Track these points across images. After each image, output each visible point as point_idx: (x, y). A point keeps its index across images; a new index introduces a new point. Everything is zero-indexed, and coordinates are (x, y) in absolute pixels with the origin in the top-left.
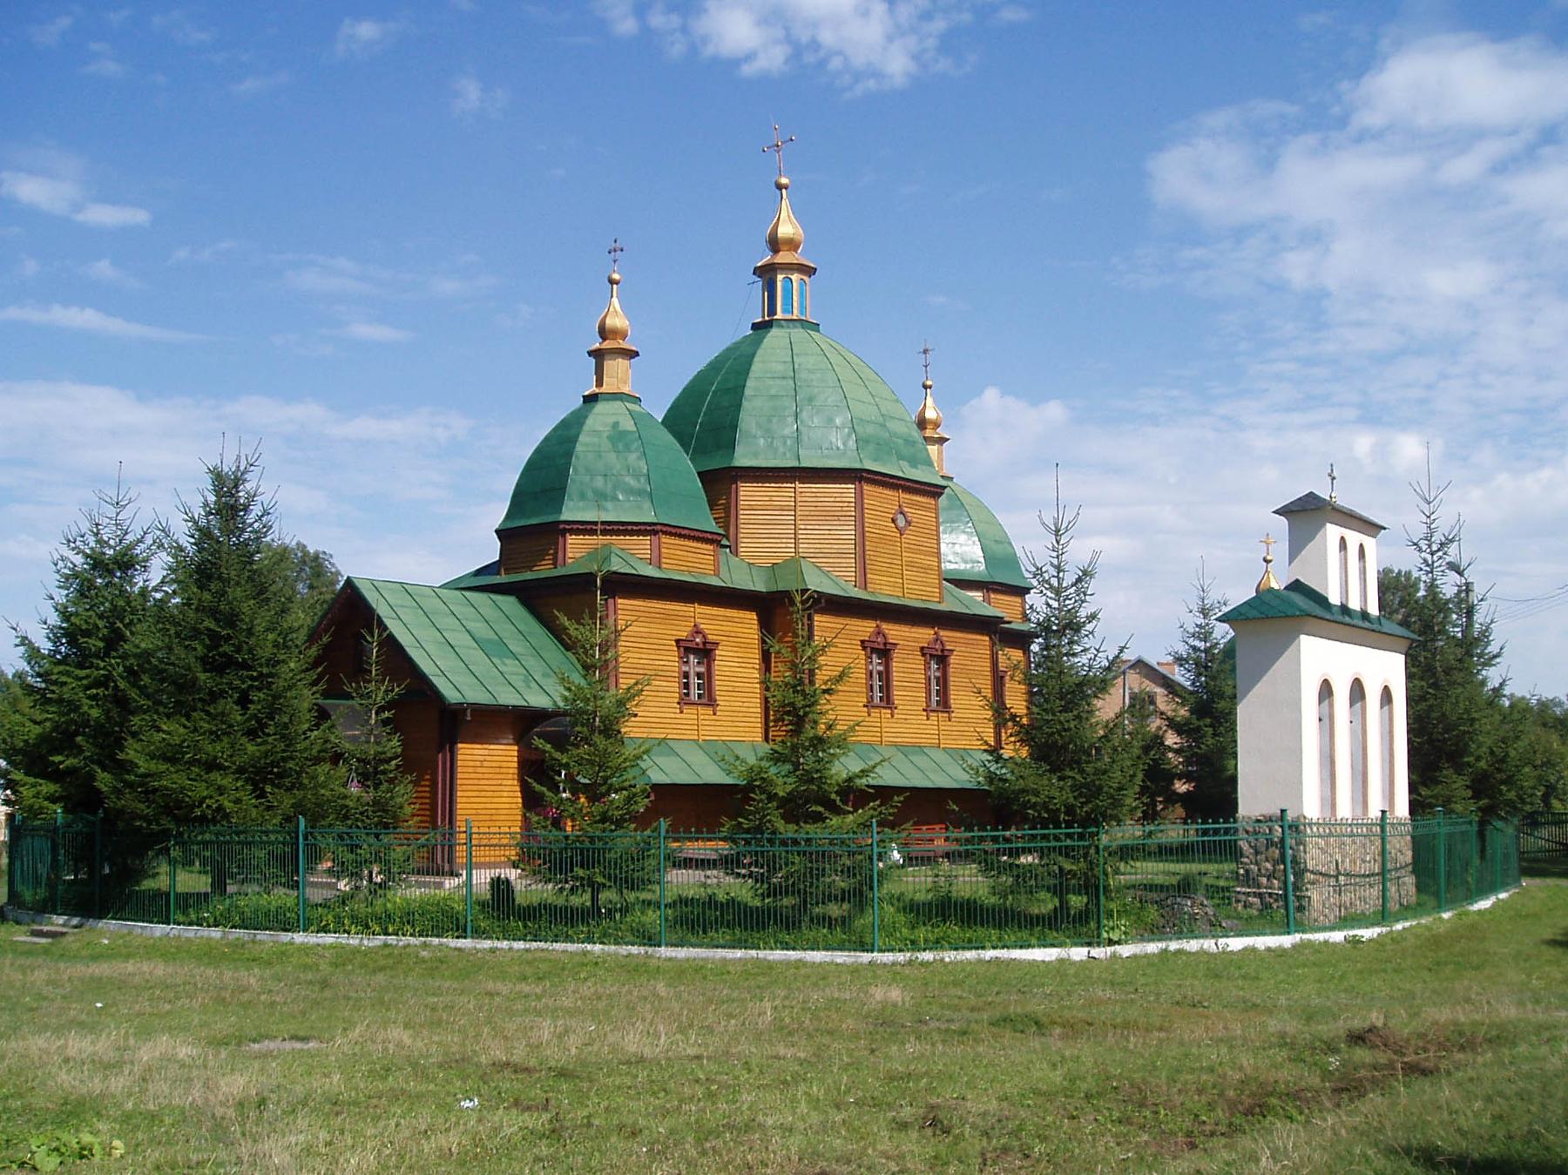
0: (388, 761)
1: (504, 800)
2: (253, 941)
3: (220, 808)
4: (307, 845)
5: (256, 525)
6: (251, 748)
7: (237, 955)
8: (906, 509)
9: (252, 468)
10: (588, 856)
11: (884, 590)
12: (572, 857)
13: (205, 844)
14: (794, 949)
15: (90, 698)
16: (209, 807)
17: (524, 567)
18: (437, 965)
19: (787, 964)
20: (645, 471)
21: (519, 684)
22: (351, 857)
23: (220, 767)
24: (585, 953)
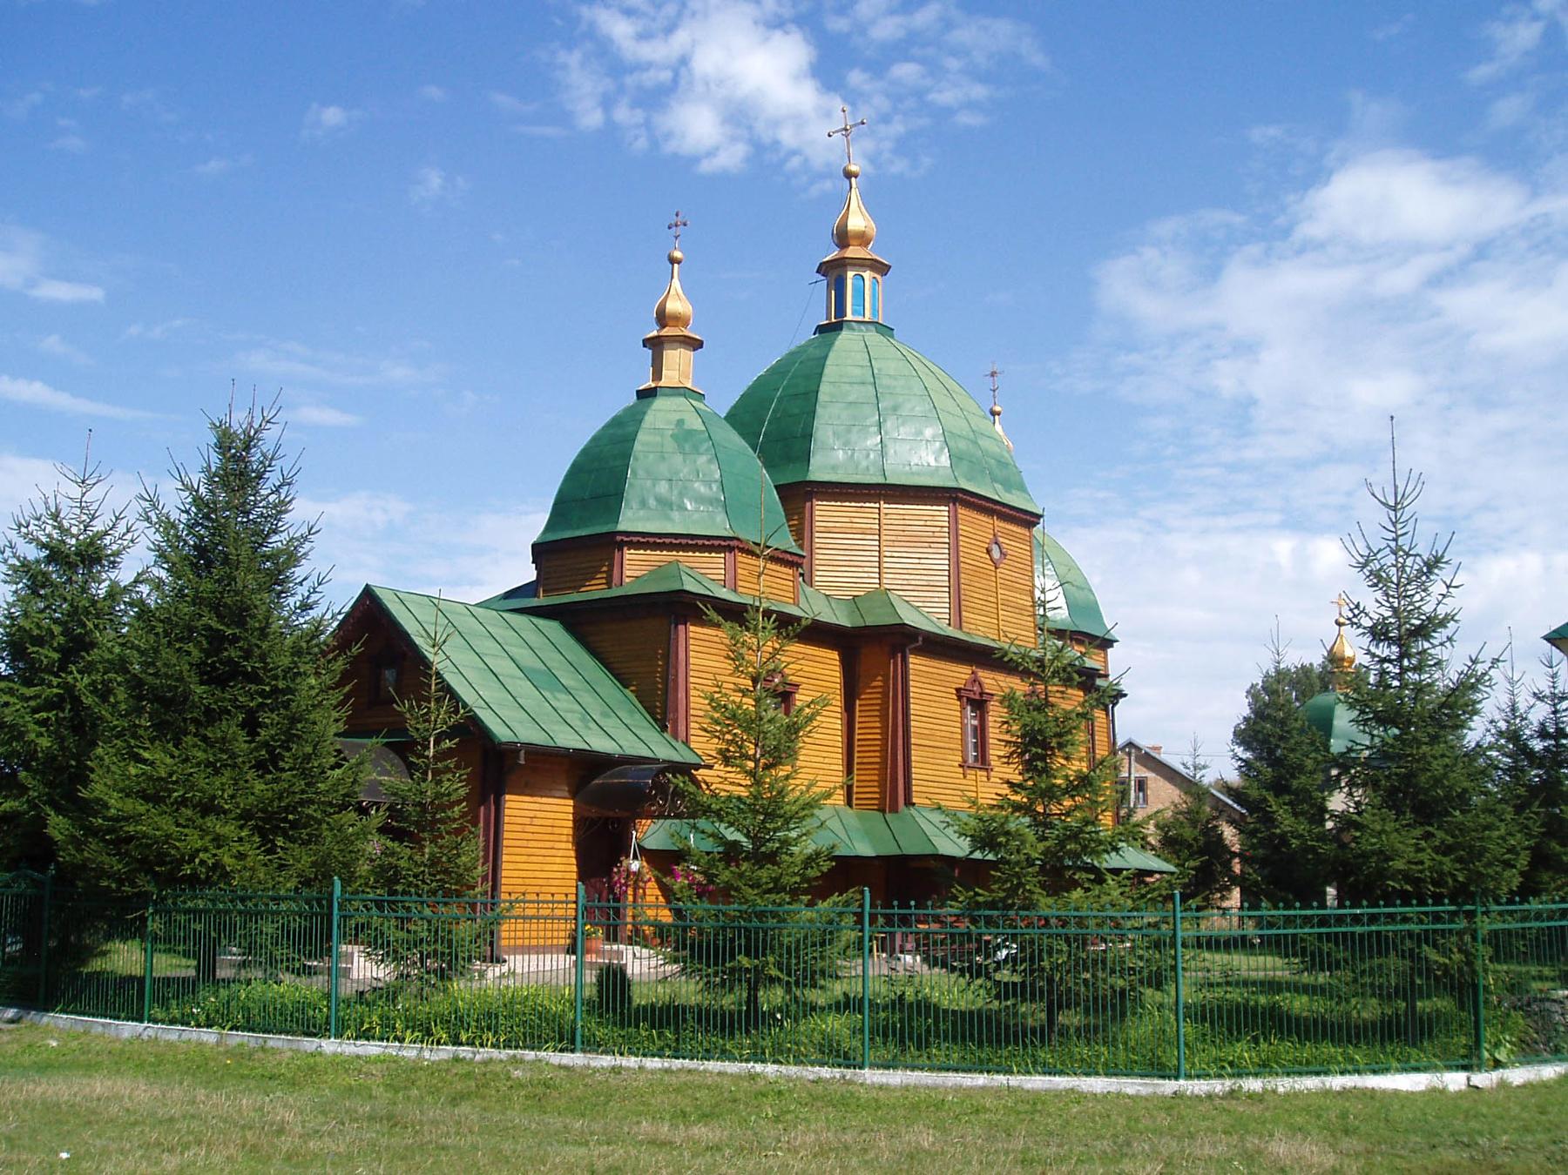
0: (452, 805)
1: (555, 867)
2: (263, 1049)
3: (217, 865)
4: (345, 917)
5: (272, 498)
6: (259, 786)
7: (241, 1070)
8: (1001, 540)
9: (269, 426)
10: (757, 940)
11: (979, 630)
12: (732, 940)
13: (196, 913)
14: (1061, 1073)
15: (39, 723)
16: (202, 862)
17: (570, 588)
18: (541, 1092)
19: (1058, 1095)
20: (717, 476)
21: (576, 723)
22: (402, 935)
23: (219, 811)
24: (753, 1077)
